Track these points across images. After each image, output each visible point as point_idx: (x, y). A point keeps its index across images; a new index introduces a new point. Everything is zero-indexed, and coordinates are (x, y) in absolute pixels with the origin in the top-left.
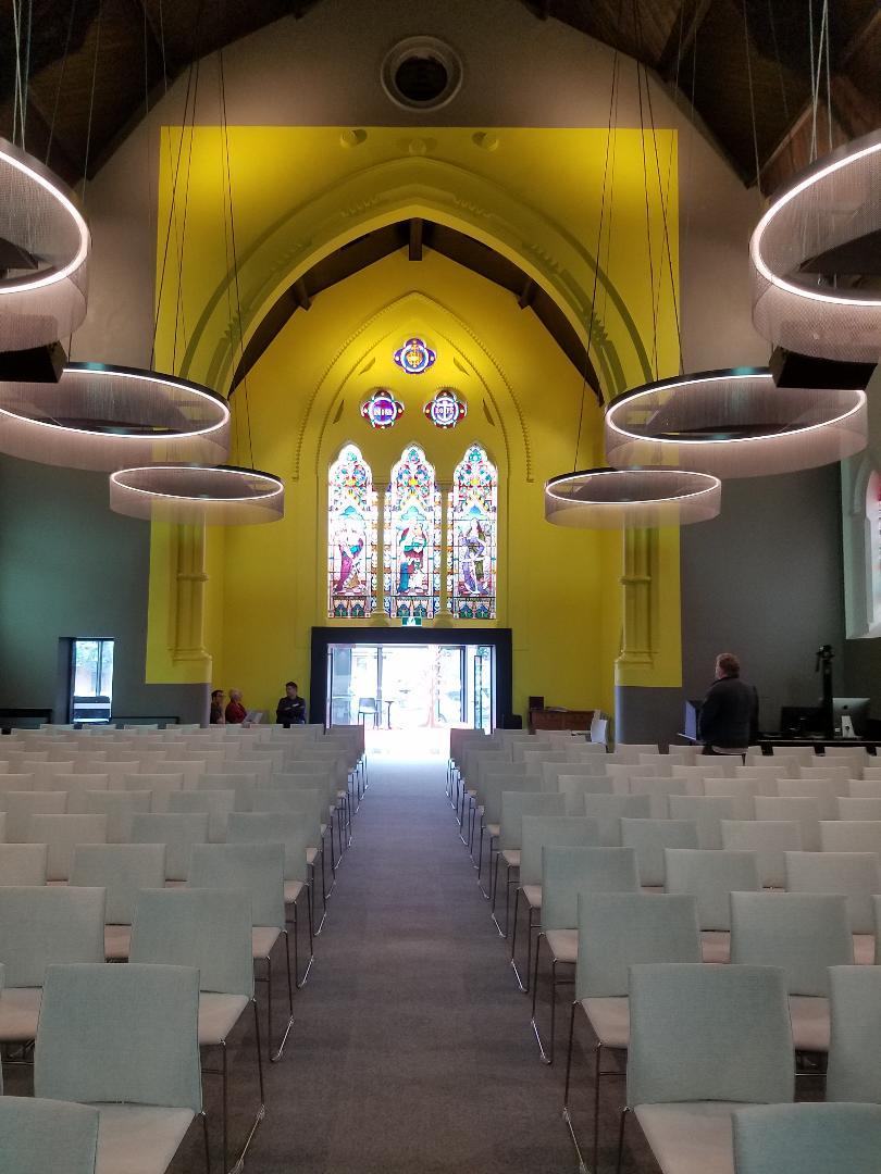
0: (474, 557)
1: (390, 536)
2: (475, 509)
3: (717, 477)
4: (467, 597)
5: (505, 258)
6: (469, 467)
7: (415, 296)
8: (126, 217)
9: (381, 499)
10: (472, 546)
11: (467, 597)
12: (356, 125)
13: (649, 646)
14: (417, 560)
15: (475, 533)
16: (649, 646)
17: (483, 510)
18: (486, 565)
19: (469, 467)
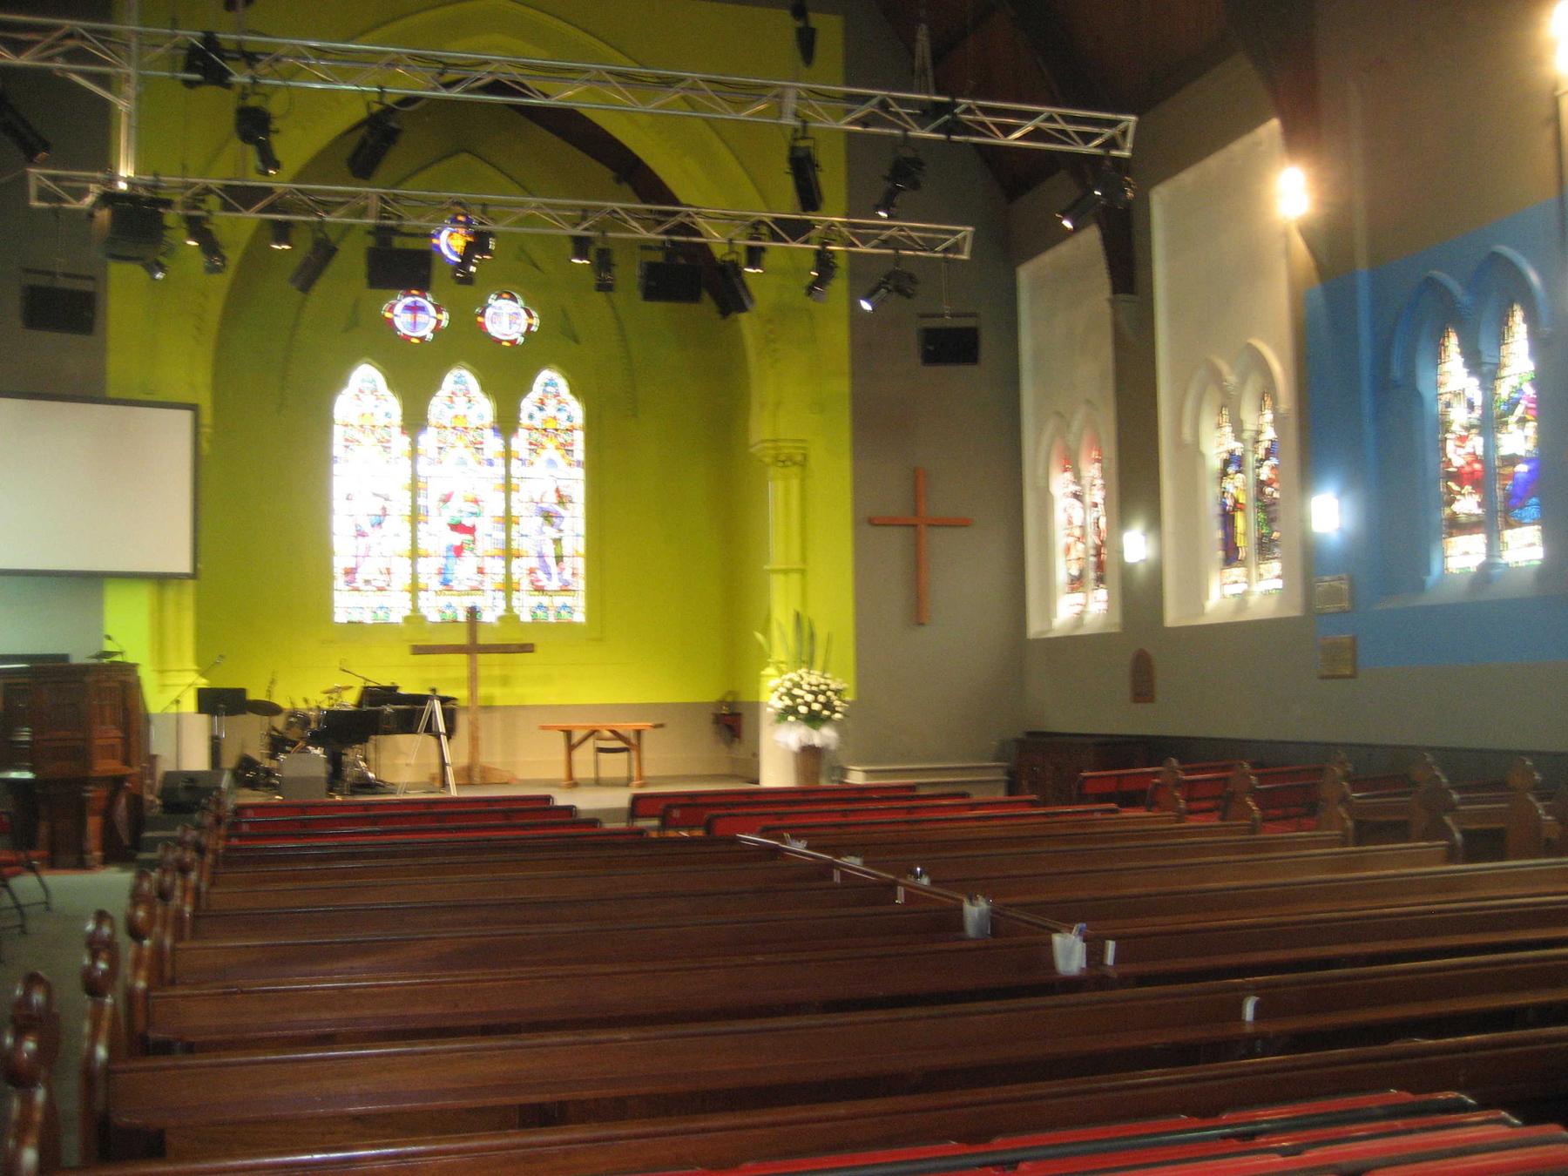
0: (551, 533)
1: (429, 501)
2: (552, 462)
3: (39, 210)
4: (540, 590)
5: (597, 127)
6: (542, 402)
7: (465, 157)
8: (489, 252)
9: (414, 444)
10: (548, 516)
11: (540, 590)
12: (867, 763)
13: (804, 560)
14: (468, 537)
15: (553, 498)
16: (804, 560)
17: (562, 463)
18: (567, 549)
19: (542, 402)
